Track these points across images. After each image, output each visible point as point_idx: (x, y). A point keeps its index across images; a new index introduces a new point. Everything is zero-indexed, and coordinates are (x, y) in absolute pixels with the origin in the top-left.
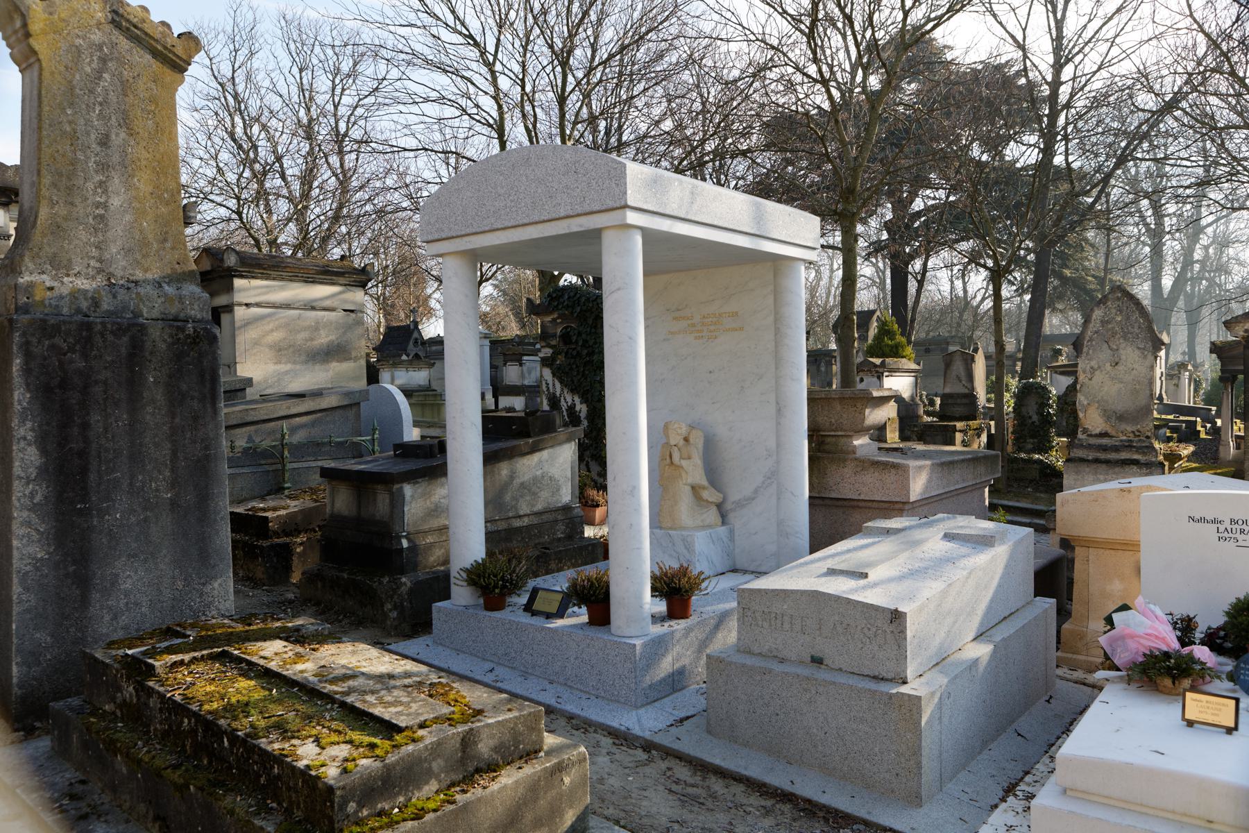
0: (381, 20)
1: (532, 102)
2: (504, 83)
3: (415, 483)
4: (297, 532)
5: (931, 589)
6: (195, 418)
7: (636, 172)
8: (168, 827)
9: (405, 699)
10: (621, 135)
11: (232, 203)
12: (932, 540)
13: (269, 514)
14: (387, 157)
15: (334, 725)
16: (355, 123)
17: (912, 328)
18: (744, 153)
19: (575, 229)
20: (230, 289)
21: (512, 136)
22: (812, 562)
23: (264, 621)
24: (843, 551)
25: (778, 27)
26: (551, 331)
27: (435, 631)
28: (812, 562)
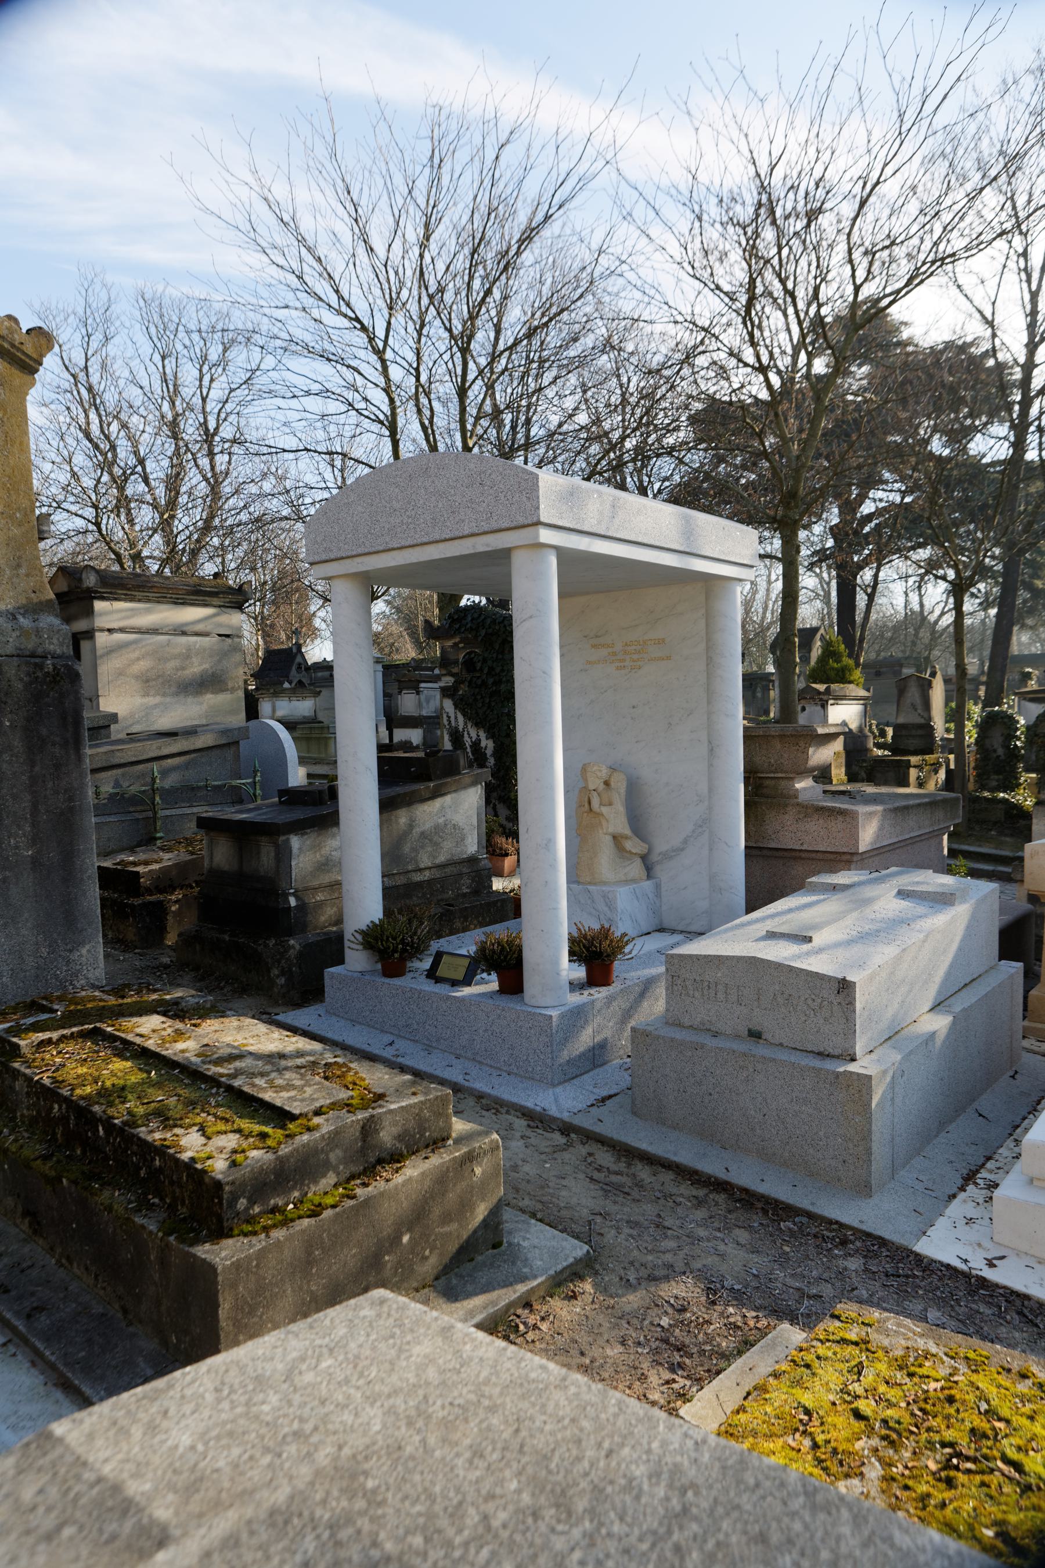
0: (254, 301)
1: (428, 394)
2: (396, 373)
3: (303, 835)
4: (171, 888)
5: (884, 954)
7: (548, 480)
8: (39, 1223)
9: (298, 1083)
10: (528, 431)
11: (90, 513)
12: (885, 900)
13: (140, 869)
14: (264, 458)
15: (220, 1111)
16: (225, 420)
17: (861, 648)
18: (670, 451)
19: (481, 549)
20: (90, 612)
21: (406, 432)
22: (749, 923)
23: (139, 992)
24: (784, 911)
25: (709, 307)
26: (452, 657)
27: (327, 1000)
28: (749, 923)
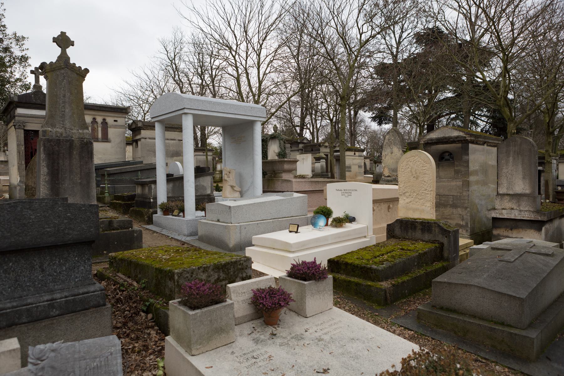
6: (86, 163)
